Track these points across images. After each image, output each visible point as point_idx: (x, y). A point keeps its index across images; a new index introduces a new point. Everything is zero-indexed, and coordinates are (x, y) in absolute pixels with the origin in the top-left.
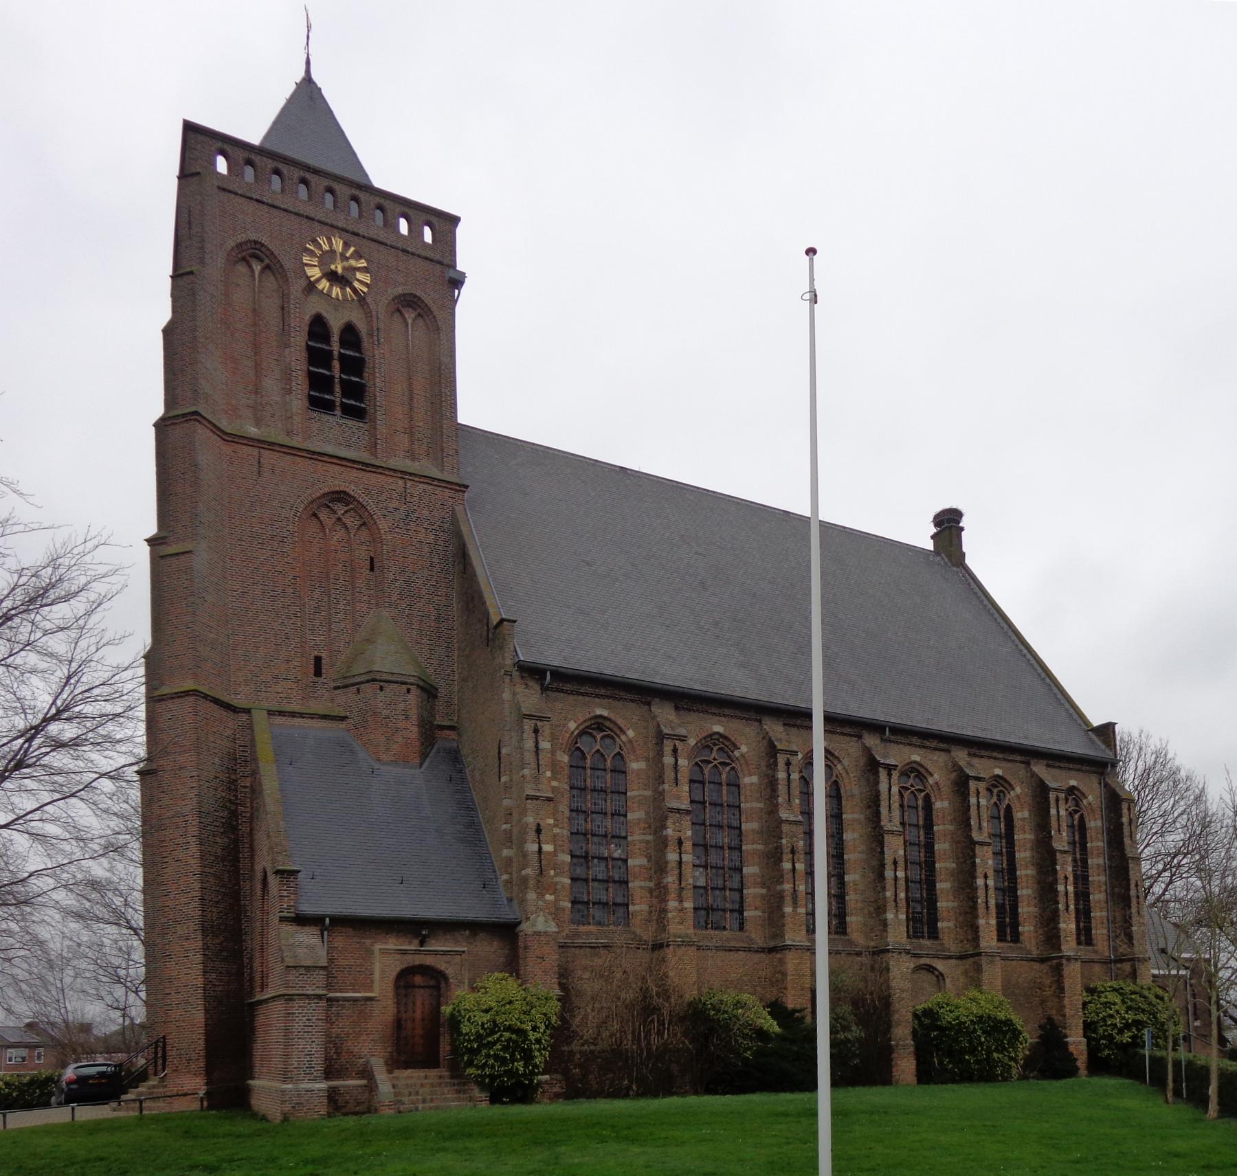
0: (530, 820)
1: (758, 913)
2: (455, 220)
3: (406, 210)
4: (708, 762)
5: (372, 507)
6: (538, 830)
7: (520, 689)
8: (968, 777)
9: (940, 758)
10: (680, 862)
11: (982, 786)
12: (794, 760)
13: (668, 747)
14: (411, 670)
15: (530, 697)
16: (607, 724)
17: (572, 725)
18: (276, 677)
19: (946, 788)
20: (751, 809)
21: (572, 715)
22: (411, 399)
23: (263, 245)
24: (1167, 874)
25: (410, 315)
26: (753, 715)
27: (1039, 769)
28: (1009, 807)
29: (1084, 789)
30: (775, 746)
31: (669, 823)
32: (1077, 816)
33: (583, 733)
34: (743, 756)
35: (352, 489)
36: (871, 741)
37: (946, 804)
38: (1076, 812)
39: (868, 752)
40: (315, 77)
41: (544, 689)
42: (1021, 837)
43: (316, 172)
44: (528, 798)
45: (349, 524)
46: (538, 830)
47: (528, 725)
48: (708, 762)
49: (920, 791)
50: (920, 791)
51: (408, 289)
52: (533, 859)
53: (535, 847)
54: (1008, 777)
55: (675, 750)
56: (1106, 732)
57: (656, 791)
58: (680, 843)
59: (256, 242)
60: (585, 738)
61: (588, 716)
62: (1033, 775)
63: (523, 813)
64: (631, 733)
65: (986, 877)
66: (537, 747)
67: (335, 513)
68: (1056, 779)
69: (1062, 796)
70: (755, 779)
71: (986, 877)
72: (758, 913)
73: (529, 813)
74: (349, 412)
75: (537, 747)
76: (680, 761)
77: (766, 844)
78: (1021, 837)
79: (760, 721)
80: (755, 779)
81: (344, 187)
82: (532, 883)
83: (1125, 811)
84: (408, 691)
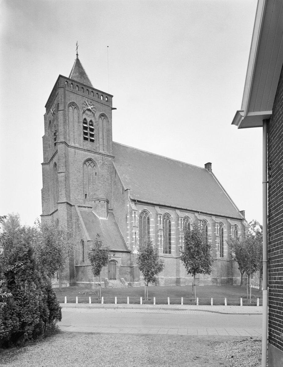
0: (134, 231)
1: (174, 250)
2: (112, 96)
3: (103, 94)
4: (165, 219)
5: (96, 162)
6: (135, 233)
7: (131, 204)
8: (216, 223)
9: (210, 218)
10: (161, 240)
11: (218, 224)
12: (161, 216)
13: (159, 216)
14: (105, 198)
15: (133, 206)
16: (146, 211)
17: (140, 211)
18: (79, 199)
19: (211, 225)
20: (173, 229)
21: (140, 208)
22: (103, 137)
23: (75, 103)
24: (144, 337)
25: (103, 118)
26: (174, 209)
27: (229, 220)
28: (222, 229)
29: (237, 225)
30: (231, 224)
31: (159, 232)
32: (236, 231)
33: (142, 213)
34: (172, 217)
35: (93, 158)
36: (196, 214)
37: (210, 228)
38: (236, 230)
39: (196, 217)
40: (79, 58)
41: (135, 204)
42: (225, 235)
43: (85, 86)
44: (133, 227)
45: (92, 165)
46: (135, 233)
47: (159, 216)
48: (165, 219)
49: (205, 225)
50: (205, 225)
51: (103, 112)
52: (134, 239)
53: (135, 237)
54: (223, 222)
55: (160, 217)
56: (242, 212)
57: (156, 225)
58: (161, 236)
59: (73, 102)
60: (142, 214)
61: (143, 209)
62: (228, 222)
63: (132, 229)
64: (151, 213)
65: (218, 244)
66: (135, 216)
67: (89, 163)
68: (233, 223)
69: (183, 219)
70: (174, 223)
71: (218, 244)
72: (174, 250)
73: (134, 230)
74: (92, 141)
75: (135, 216)
76: (180, 222)
77: (176, 236)
78: (225, 235)
79: (194, 214)
80: (174, 223)
81: (90, 89)
82: (134, 244)
83: (246, 230)
84: (100, 202)
